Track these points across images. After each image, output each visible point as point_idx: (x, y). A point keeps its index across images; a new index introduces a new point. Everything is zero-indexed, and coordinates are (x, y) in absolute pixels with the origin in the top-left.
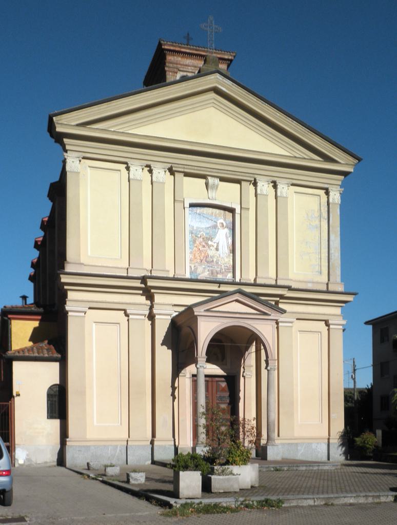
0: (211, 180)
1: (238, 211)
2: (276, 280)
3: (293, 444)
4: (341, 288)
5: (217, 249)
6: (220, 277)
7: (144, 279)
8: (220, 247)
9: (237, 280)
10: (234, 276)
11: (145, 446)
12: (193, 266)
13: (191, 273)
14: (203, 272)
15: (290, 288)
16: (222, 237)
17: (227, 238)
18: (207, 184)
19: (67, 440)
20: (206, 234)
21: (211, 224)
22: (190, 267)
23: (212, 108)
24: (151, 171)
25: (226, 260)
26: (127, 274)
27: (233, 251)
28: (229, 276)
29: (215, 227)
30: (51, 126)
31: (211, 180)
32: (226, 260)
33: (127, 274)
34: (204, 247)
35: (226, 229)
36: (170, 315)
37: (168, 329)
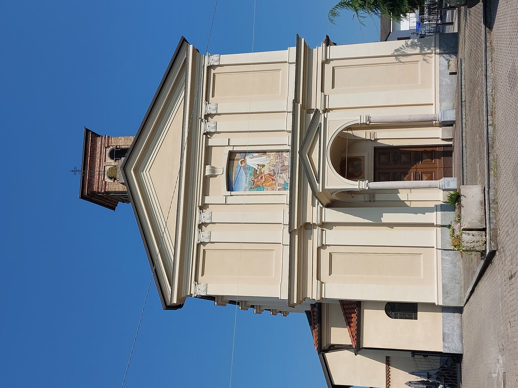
0: (207, 173)
1: (231, 149)
2: (291, 63)
3: (440, 90)
4: (293, 49)
5: (263, 166)
6: (287, 163)
7: (291, 232)
8: (261, 163)
9: (289, 148)
10: (287, 151)
11: (442, 233)
12: (279, 188)
13: (285, 189)
14: (283, 178)
15: (296, 101)
16: (252, 161)
17: (253, 157)
18: (211, 176)
19: (437, 304)
20: (458, 293)
21: (242, 171)
22: (279, 190)
23: (145, 175)
24: (205, 224)
25: (272, 158)
26: (288, 245)
27: (264, 152)
28: (287, 156)
29: (245, 168)
30: (175, 307)
31: (207, 173)
32: (272, 158)
33: (288, 245)
34: (262, 177)
35: (246, 158)
36: (321, 208)
37: (339, 211)
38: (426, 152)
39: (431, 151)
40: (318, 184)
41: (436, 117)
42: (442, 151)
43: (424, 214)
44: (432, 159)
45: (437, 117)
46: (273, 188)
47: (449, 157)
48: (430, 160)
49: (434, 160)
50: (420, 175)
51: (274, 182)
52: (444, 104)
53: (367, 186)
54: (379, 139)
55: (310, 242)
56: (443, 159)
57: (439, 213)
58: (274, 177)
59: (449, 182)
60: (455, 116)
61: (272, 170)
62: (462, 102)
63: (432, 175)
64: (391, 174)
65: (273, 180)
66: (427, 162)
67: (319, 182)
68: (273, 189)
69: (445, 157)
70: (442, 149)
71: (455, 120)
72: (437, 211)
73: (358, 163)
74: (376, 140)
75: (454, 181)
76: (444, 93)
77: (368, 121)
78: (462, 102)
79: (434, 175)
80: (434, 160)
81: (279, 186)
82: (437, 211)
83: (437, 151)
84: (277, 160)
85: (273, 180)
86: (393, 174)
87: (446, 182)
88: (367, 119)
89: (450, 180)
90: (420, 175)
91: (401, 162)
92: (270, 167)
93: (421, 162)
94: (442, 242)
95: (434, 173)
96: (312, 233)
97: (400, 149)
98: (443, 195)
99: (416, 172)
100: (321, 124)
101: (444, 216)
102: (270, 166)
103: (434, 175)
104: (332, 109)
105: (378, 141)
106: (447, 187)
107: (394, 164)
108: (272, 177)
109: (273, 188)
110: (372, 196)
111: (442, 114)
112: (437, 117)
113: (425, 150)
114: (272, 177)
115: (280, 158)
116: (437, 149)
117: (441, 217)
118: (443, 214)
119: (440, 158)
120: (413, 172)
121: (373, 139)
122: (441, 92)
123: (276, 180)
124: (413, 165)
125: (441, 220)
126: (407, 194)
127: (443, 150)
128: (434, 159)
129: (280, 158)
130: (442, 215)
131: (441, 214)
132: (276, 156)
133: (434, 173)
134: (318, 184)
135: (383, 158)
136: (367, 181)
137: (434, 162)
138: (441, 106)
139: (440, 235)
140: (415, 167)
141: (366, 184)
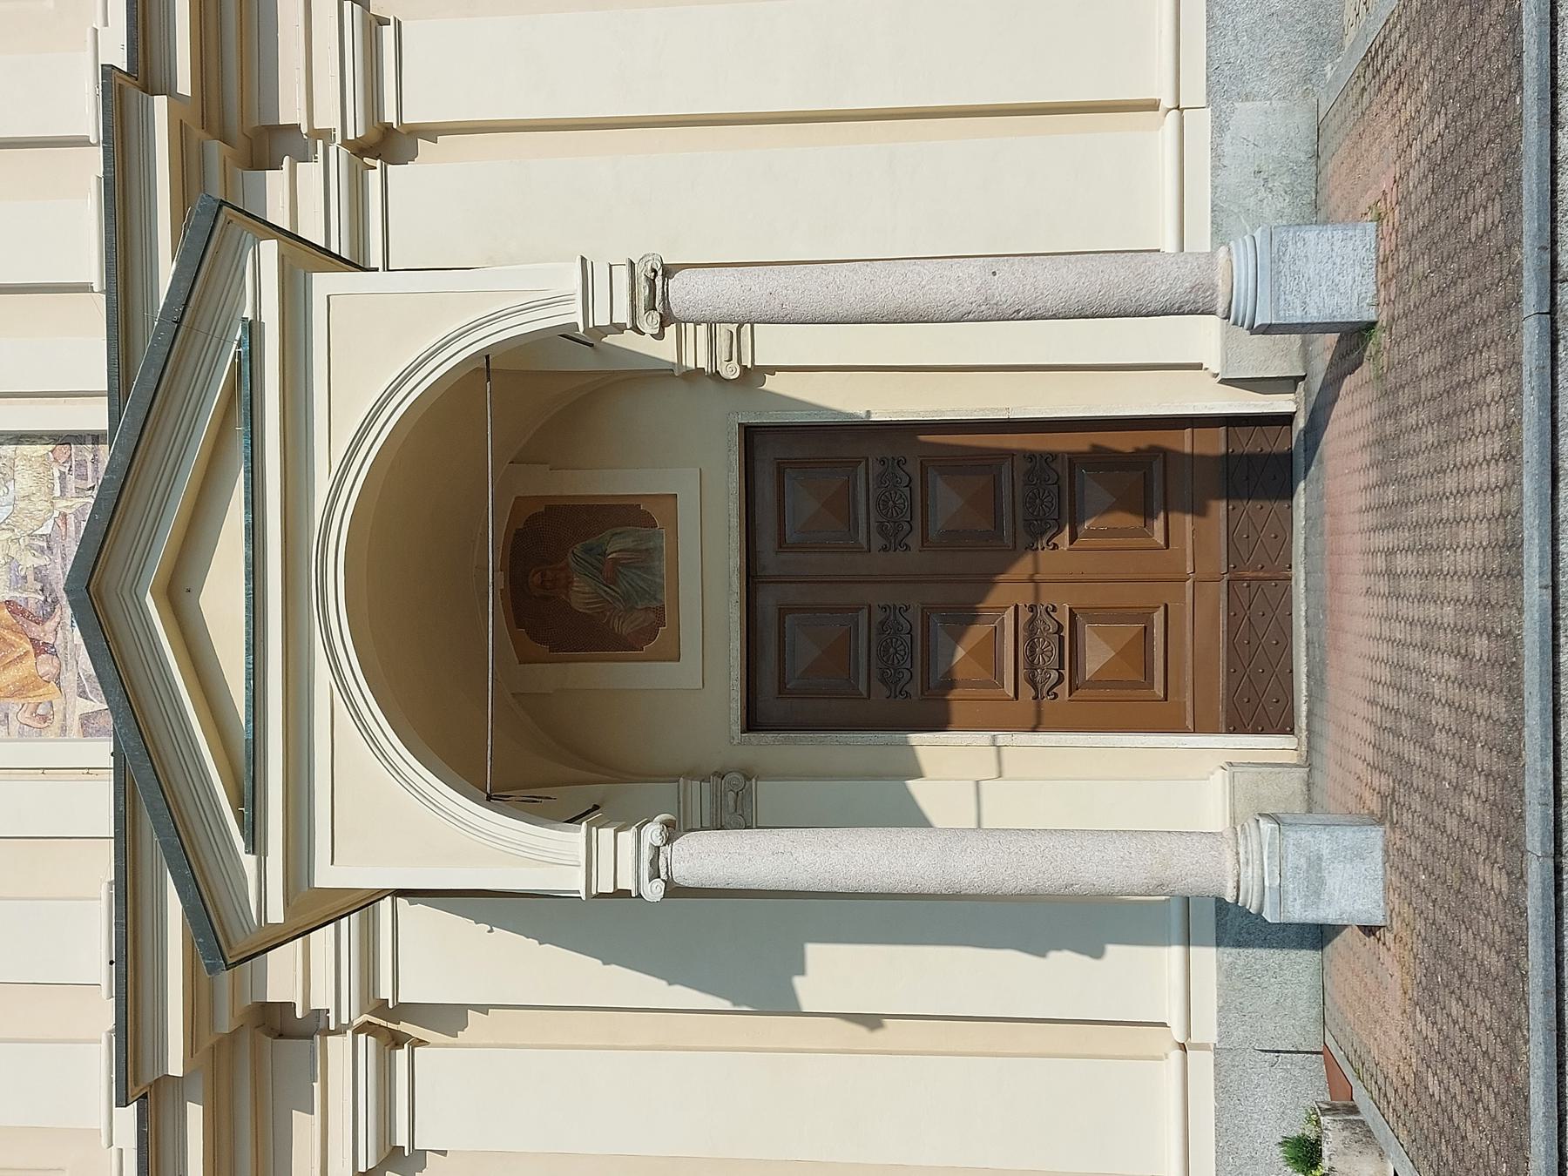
32: (24, 481)
38: (1101, 460)
39: (1138, 450)
40: (249, 862)
41: (1214, 287)
42: (1216, 459)
43: (1097, 953)
44: (1149, 515)
45: (1222, 289)
46: (40, 711)
47: (1267, 504)
48: (1134, 521)
49: (1158, 524)
50: (1066, 633)
51: (46, 666)
52: (1247, 116)
53: (655, 874)
54: (773, 370)
55: (304, 1127)
56: (1223, 512)
57: (1207, 958)
58: (50, 625)
59: (1315, 863)
60: (1370, 280)
61: (31, 578)
62: (1553, 281)
63: (1147, 632)
64: (863, 617)
65: (40, 648)
66: (1112, 532)
67: (255, 841)
68: (44, 718)
69: (1237, 503)
70: (1214, 443)
71: (1369, 315)
72: (1187, 943)
73: (629, 543)
74: (752, 375)
75: (1358, 855)
76: (1244, 20)
77: (651, 307)
78: (1553, 281)
79: (1158, 631)
80: (1158, 524)
81: (83, 694)
82: (1187, 943)
83: (1184, 455)
84: (61, 504)
85: (40, 648)
86: (878, 616)
87: (1292, 860)
88: (643, 292)
89: (1325, 852)
90: (1060, 627)
91: (932, 535)
92: (12, 553)
93: (1073, 537)
94: (1220, 1153)
95: (1158, 617)
96: (313, 1069)
97: (922, 438)
98: (1233, 805)
99: (1032, 608)
100: (253, 329)
101: (1239, 985)
102: (14, 548)
103: (1158, 631)
104: (431, 132)
105: (772, 384)
106: (1305, 906)
107: (885, 549)
108: (35, 631)
109: (40, 711)
110: (731, 795)
111: (1264, 260)
112: (1222, 289)
113: (1094, 446)
114: (35, 631)
115: (81, 484)
116: (1185, 442)
117: (1220, 986)
118: (1233, 965)
119: (1198, 509)
120: (1017, 607)
121: (730, 371)
122: (1217, 12)
123: (60, 650)
124: (1014, 554)
125: (1220, 1009)
126: (972, 785)
127: (1223, 450)
128: (1162, 515)
129: (81, 484)
130: (1226, 973)
131: (1219, 967)
132: (57, 474)
133: (1158, 617)
134: (249, 862)
135: (804, 503)
136: (653, 833)
137: (1159, 538)
138: (1219, 128)
139: (1212, 1103)
140: (1024, 566)
141: (646, 855)
